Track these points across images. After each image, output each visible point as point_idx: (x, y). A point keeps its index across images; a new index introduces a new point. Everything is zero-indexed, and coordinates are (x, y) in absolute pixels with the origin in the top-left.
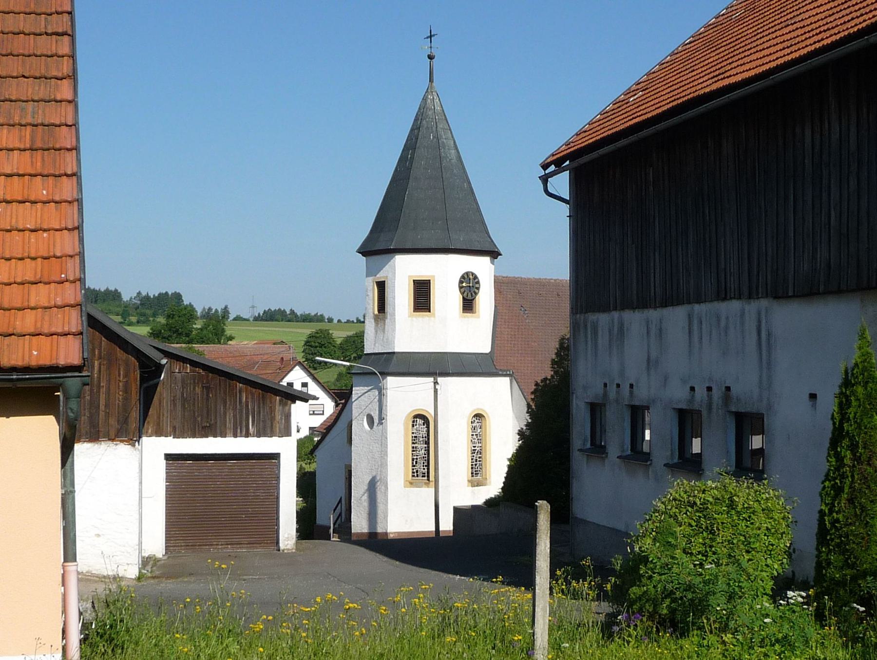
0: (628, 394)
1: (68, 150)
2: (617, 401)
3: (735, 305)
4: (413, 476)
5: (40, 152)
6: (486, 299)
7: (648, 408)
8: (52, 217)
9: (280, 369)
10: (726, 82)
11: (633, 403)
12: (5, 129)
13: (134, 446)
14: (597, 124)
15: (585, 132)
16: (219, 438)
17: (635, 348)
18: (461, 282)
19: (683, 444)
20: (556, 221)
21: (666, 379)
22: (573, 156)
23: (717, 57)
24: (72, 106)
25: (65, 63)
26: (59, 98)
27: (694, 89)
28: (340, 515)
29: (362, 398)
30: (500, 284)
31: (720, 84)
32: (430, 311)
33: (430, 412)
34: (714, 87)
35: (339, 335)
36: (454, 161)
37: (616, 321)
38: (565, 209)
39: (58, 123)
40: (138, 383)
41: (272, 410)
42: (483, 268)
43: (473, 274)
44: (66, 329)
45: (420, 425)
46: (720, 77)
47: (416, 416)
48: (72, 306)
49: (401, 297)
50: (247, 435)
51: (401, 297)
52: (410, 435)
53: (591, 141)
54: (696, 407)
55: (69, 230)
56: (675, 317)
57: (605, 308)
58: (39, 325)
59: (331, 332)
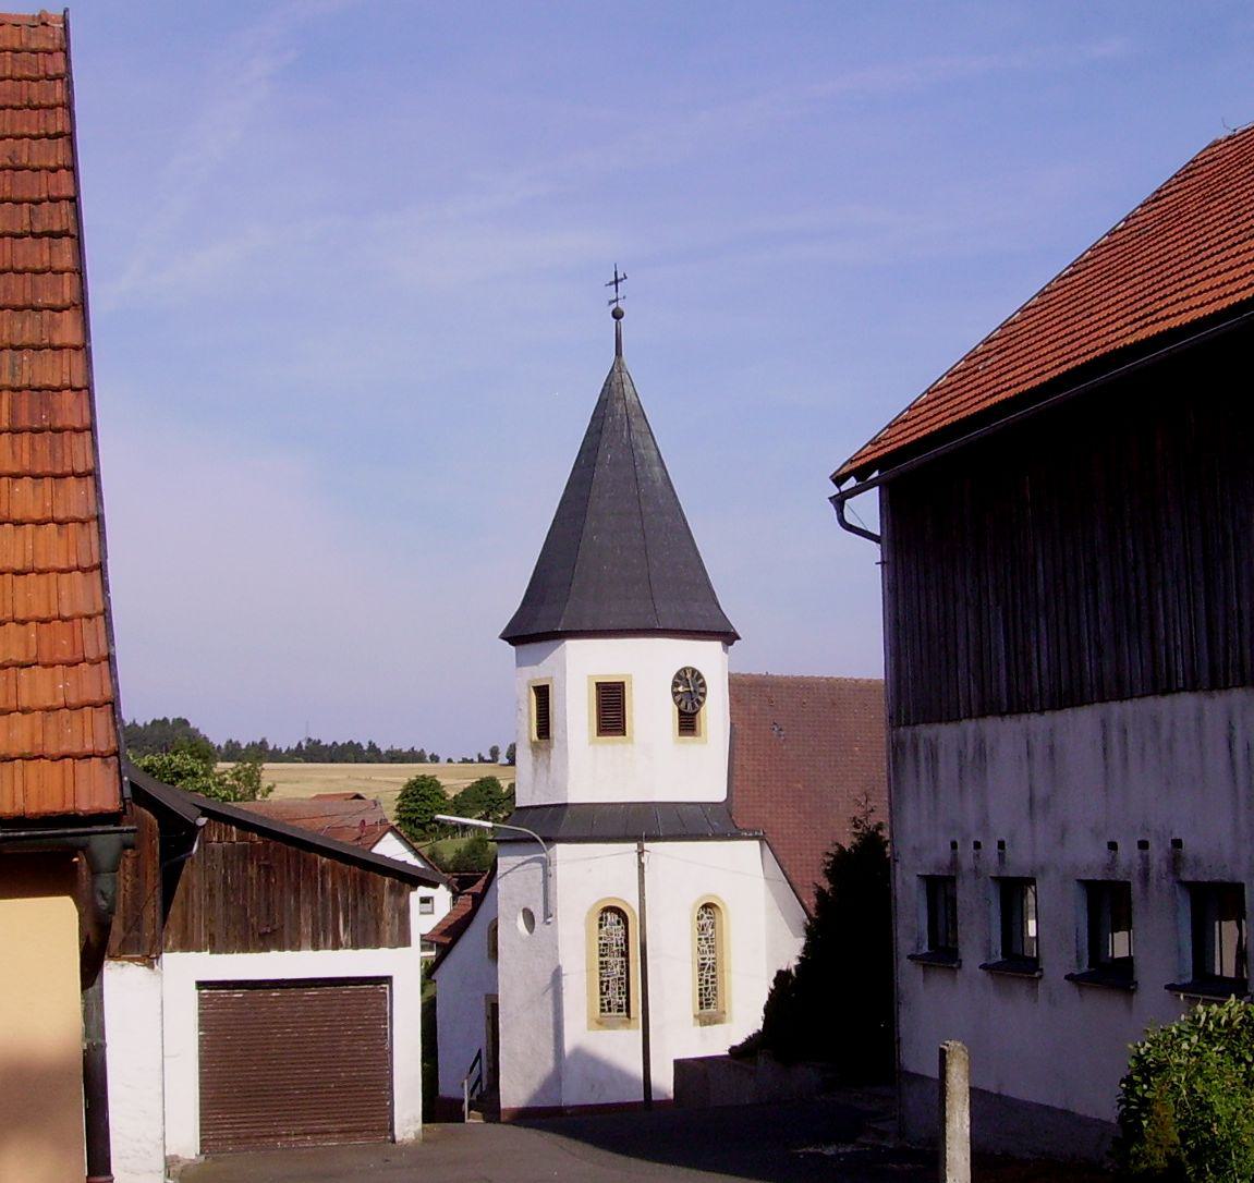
0: (996, 858)
1: (76, 431)
2: (976, 872)
3: (1186, 702)
4: (603, 1011)
5: (27, 436)
6: (716, 712)
7: (1031, 881)
8: (52, 547)
9: (359, 838)
10: (1162, 327)
11: (1005, 874)
12: (7, 354)
13: (153, 967)
14: (925, 408)
15: (905, 421)
16: (288, 953)
17: (1007, 780)
18: (675, 685)
19: (1097, 943)
20: (861, 570)
21: (1064, 830)
22: (881, 463)
23: (1131, 292)
24: (80, 354)
25: (67, 282)
26: (57, 342)
27: (1103, 341)
28: (479, 1079)
29: (514, 877)
30: (742, 689)
31: (1152, 331)
33: (631, 903)
34: (1142, 335)
35: (454, 783)
36: (659, 483)
37: (971, 740)
38: (874, 551)
39: (57, 384)
40: (157, 859)
41: (378, 903)
42: (708, 658)
44: (89, 747)
45: (612, 924)
46: (1149, 319)
47: (606, 910)
48: (95, 705)
49: (576, 711)
50: (337, 946)
51: (576, 711)
52: (596, 942)
53: (920, 434)
54: (1120, 876)
55: (84, 570)
56: (1079, 725)
57: (951, 716)
58: (38, 739)
59: (437, 779)
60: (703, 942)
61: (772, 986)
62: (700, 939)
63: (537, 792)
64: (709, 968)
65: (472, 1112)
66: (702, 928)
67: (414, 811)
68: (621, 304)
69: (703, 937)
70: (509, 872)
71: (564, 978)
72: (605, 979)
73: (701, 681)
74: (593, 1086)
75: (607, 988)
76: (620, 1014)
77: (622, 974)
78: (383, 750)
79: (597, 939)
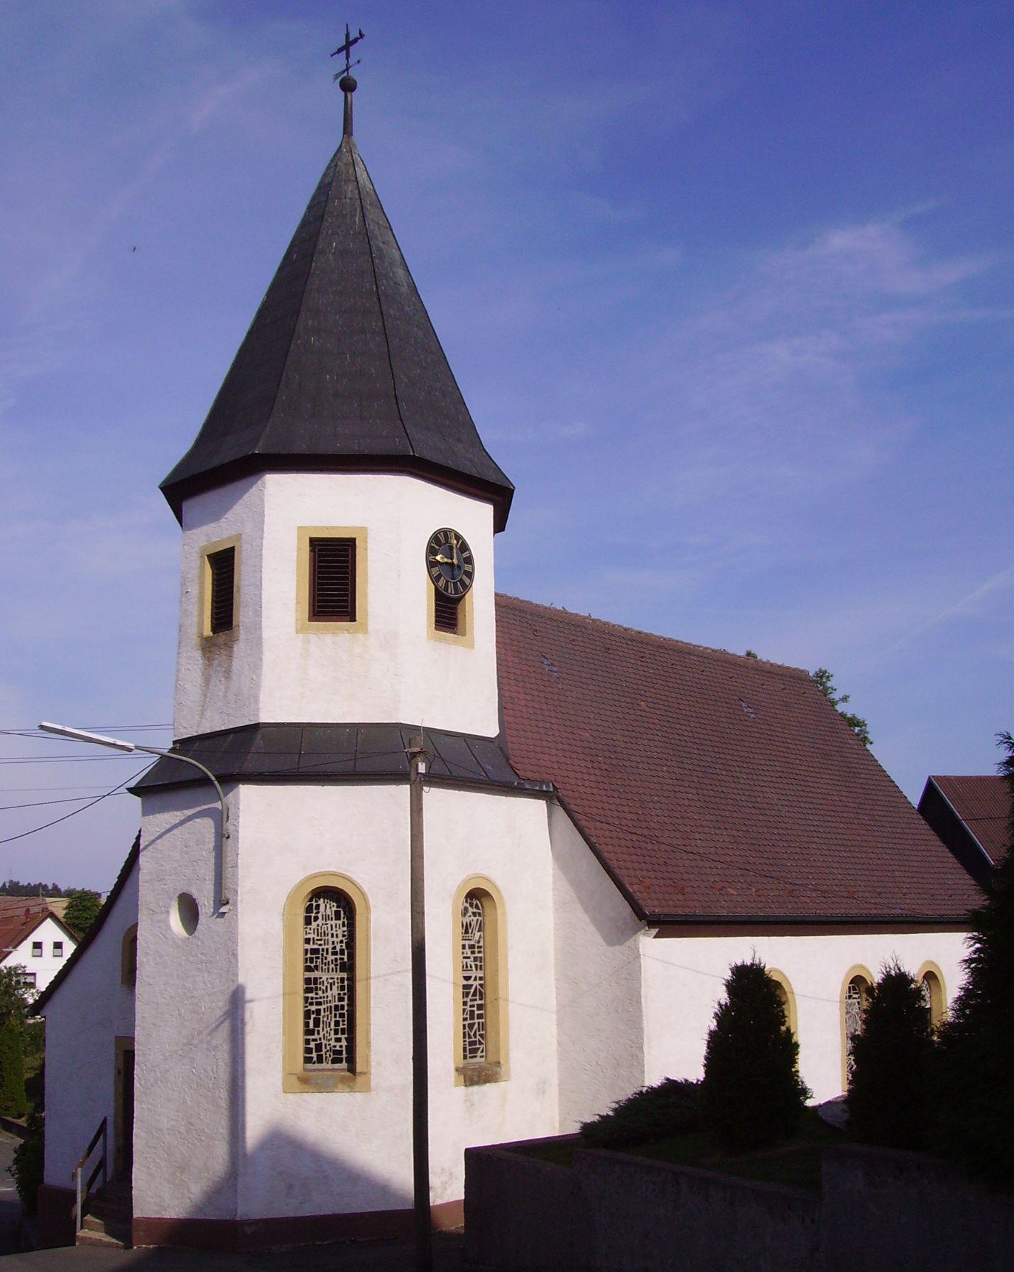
18: (431, 551)
28: (102, 1164)
32: (353, 619)
36: (404, 289)
43: (458, 537)
45: (326, 918)
49: (278, 583)
51: (278, 583)
52: (300, 947)
60: (468, 951)
61: (723, 997)
62: (464, 947)
63: (208, 713)
64: (474, 994)
65: (89, 1217)
66: (467, 929)
67: (77, 918)
68: (353, 73)
69: (467, 943)
70: (160, 837)
71: (248, 1006)
72: (313, 1008)
73: (466, 555)
74: (291, 1186)
75: (317, 1022)
76: (337, 1066)
77: (341, 999)
78: (63, 890)
79: (302, 941)
